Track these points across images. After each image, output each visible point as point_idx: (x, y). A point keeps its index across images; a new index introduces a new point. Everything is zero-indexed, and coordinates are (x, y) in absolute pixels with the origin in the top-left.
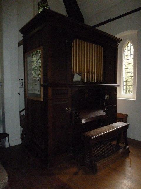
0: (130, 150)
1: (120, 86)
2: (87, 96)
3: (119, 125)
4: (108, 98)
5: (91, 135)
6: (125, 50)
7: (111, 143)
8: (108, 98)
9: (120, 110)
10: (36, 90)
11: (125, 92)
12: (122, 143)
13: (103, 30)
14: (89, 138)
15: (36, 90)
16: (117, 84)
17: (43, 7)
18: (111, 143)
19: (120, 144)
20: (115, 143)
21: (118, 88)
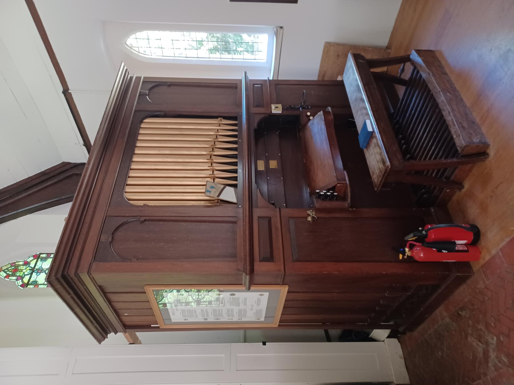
0: (424, 47)
1: (245, 73)
2: (273, 164)
3: (352, 79)
4: (280, 106)
5: (381, 166)
6: (148, 53)
7: (401, 98)
8: (280, 106)
9: (307, 66)
10: (259, 300)
11: (255, 53)
12: (403, 70)
13: (361, 128)
14: (388, 174)
15: (259, 300)
16: (241, 80)
17: (31, 274)
18: (401, 98)
19: (407, 76)
20: (401, 90)
21: (252, 77)
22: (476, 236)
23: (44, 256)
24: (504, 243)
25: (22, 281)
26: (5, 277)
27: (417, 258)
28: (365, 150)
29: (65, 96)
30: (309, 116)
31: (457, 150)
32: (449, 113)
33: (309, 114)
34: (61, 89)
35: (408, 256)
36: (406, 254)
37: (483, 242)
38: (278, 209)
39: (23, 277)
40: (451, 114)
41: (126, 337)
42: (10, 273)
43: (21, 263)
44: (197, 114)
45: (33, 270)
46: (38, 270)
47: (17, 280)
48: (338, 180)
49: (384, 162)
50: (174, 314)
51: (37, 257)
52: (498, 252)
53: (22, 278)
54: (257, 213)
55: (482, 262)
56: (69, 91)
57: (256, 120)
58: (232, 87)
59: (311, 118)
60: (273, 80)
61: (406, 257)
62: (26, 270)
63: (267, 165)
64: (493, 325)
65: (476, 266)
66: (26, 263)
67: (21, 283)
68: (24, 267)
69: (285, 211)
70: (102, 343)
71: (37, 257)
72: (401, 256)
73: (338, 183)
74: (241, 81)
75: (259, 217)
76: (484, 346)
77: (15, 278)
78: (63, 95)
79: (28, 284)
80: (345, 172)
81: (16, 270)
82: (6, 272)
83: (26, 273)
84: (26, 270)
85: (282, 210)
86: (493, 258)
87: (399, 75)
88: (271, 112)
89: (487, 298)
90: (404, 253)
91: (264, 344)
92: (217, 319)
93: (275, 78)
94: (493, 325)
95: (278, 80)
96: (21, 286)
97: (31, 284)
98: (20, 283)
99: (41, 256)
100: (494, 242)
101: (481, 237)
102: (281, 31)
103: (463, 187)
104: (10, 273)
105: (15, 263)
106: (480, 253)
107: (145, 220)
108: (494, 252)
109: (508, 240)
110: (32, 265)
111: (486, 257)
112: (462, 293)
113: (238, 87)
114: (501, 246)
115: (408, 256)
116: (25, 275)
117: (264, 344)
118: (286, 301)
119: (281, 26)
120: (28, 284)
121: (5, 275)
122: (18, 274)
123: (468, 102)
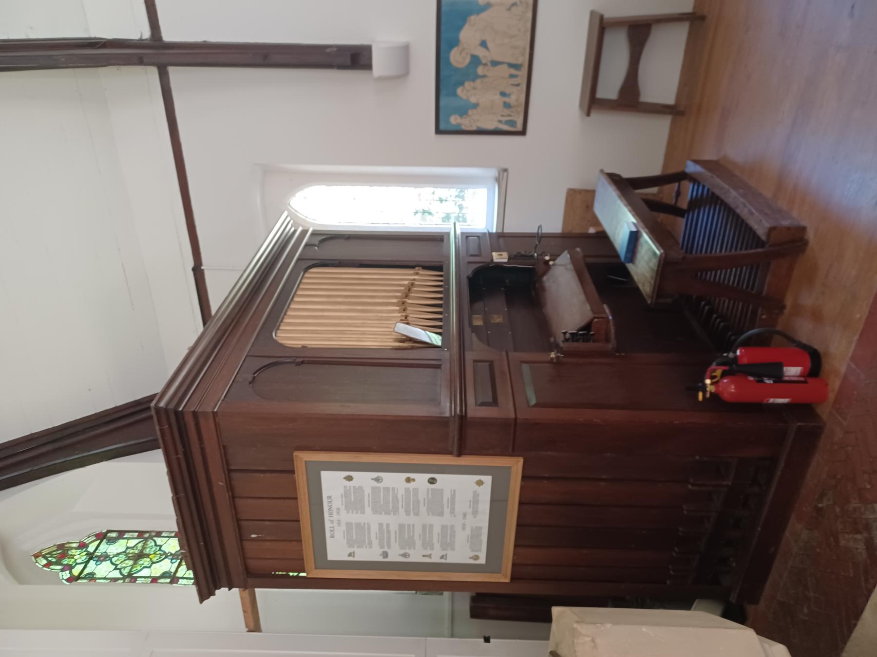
12: (678, 194)
17: (87, 563)
22: (815, 362)
23: (114, 535)
24: (853, 345)
25: (71, 572)
26: (45, 566)
27: (726, 396)
28: (630, 266)
29: (195, 274)
30: (547, 262)
31: (759, 238)
32: (744, 204)
33: (547, 258)
34: (191, 264)
35: (711, 393)
36: (708, 389)
37: (826, 366)
38: (504, 353)
39: (74, 567)
40: (747, 205)
41: (242, 598)
42: (54, 560)
43: (74, 545)
44: (385, 263)
45: (91, 556)
46: (99, 557)
47: (62, 570)
48: (594, 313)
49: (655, 254)
50: (331, 514)
51: (101, 537)
52: (849, 366)
53: (70, 568)
54: (470, 356)
55: (832, 396)
56: (202, 268)
57: (469, 271)
58: (438, 239)
59: (551, 263)
60: (497, 233)
61: (708, 395)
62: (80, 556)
63: (486, 321)
64: (868, 487)
65: (824, 411)
66: (83, 546)
67: (69, 576)
68: (79, 551)
69: (513, 355)
70: (205, 602)
71: (101, 537)
72: (700, 396)
73: (595, 318)
74: (448, 234)
75: (475, 361)
76: (865, 535)
77: (60, 567)
78: (191, 274)
79: (78, 578)
80: (605, 306)
81: (64, 555)
82: (46, 558)
83: (78, 561)
84: (80, 556)
85: (509, 353)
86: (845, 378)
87: (674, 202)
88: (492, 260)
89: (850, 448)
90: (704, 388)
91: (487, 640)
92: (408, 480)
93: (500, 231)
94: (868, 487)
95: (503, 233)
96: (68, 580)
97: (84, 578)
98: (66, 575)
99: (109, 535)
100: (840, 349)
101: (823, 360)
102: (505, 174)
103: (784, 307)
104: (54, 560)
105: (63, 544)
106: (827, 385)
107: (302, 362)
108: (843, 369)
109: (856, 337)
110: (91, 549)
111: (835, 384)
112: (819, 468)
113: (445, 240)
114: (850, 354)
115: (711, 393)
116: (77, 564)
117: (487, 640)
118: (521, 503)
119: (505, 166)
120: (78, 578)
121: (44, 562)
122: (65, 561)
123: (768, 194)
